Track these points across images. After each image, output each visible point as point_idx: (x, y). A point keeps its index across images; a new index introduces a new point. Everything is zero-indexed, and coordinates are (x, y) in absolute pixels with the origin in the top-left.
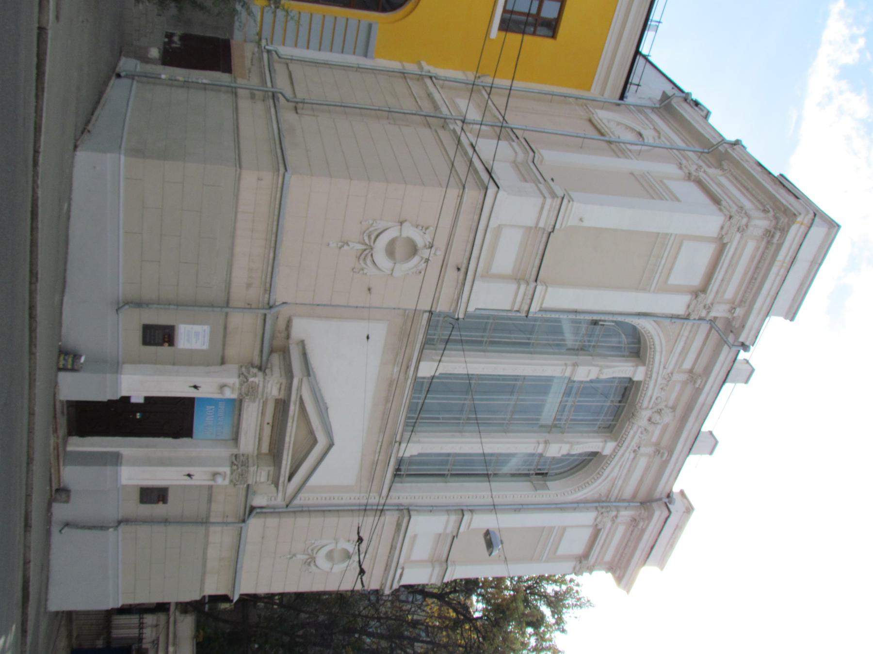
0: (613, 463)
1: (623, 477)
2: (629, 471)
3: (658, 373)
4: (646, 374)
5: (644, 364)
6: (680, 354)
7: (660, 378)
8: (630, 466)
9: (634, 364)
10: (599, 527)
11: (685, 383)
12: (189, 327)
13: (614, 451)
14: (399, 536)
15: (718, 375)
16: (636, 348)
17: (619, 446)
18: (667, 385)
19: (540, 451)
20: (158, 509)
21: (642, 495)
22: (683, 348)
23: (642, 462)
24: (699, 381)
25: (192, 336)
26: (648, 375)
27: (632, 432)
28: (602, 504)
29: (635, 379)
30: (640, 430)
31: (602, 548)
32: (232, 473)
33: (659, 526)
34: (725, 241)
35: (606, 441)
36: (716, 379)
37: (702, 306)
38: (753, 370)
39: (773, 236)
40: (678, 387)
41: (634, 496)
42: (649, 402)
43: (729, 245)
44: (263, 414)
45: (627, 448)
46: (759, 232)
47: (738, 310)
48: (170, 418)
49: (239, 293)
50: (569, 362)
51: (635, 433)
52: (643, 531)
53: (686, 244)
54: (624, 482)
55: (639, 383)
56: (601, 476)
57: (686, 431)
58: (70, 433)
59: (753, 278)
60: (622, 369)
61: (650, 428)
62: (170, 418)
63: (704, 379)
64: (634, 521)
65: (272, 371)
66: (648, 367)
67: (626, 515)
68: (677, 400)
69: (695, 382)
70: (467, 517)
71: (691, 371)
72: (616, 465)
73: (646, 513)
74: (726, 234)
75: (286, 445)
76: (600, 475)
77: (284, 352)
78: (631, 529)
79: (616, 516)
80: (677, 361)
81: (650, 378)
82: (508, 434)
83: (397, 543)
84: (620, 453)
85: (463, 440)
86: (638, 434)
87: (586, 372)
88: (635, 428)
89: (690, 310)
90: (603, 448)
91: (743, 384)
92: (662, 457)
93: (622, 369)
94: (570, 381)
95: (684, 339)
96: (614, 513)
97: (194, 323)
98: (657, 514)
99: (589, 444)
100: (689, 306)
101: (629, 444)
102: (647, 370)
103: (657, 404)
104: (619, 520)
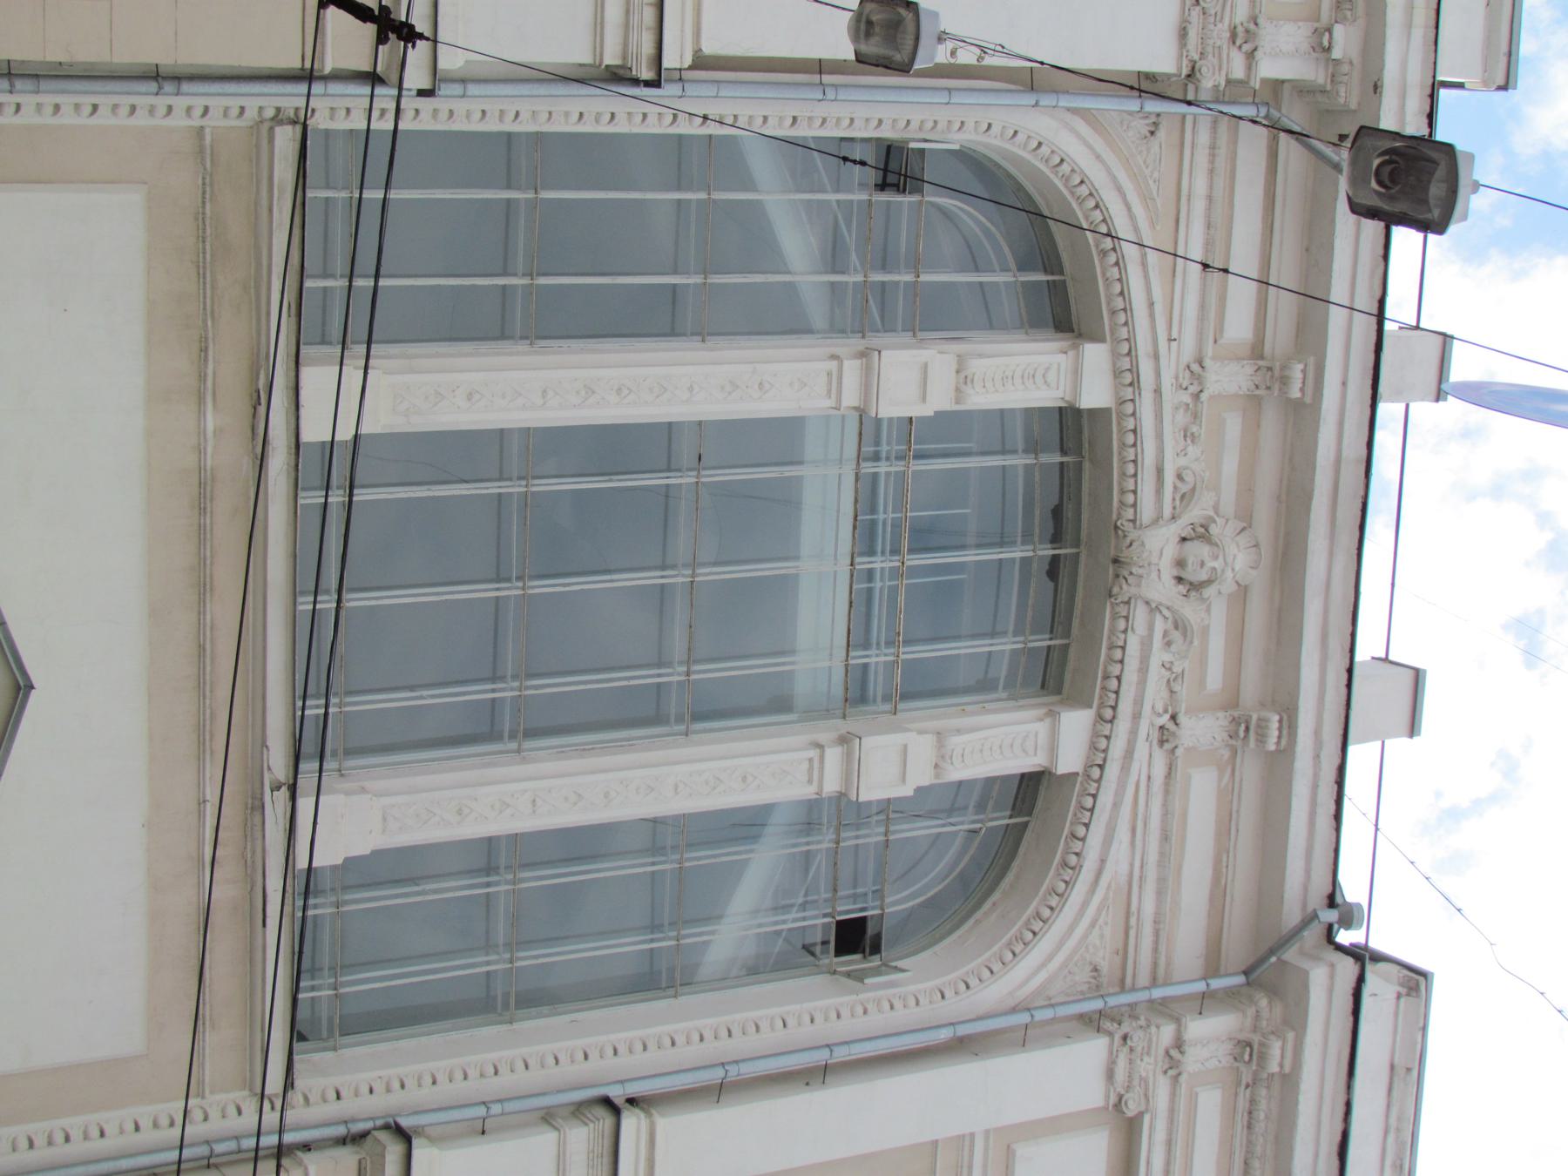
1: (1152, 874)
2: (1165, 838)
4: (1117, 373)
5: (1098, 338)
7: (1170, 360)
8: (1166, 813)
10: (1132, 1109)
11: (1253, 403)
13: (1093, 747)
15: (1317, 733)
16: (1052, 273)
17: (1105, 720)
18: (1196, 416)
19: (831, 785)
21: (1237, 949)
23: (1202, 788)
26: (1126, 375)
28: (1107, 1009)
29: (1086, 402)
34: (1130, 1114)
37: (1223, 30)
38: (1418, 676)
39: (1263, 1058)
40: (1234, 426)
41: (1212, 968)
43: (1147, 1118)
45: (1137, 716)
47: (1338, 30)
50: (823, 737)
51: (1146, 644)
52: (1289, 1082)
53: (1022, 1151)
54: (1160, 894)
56: (1076, 869)
57: (1301, 700)
60: (1023, 374)
64: (1247, 1050)
66: (1117, 341)
67: (1210, 1034)
68: (1247, 488)
69: (1284, 381)
70: (632, 1122)
71: (1257, 351)
72: (1116, 805)
73: (1278, 1010)
74: (1128, 1088)
78: (1242, 1104)
79: (1179, 1044)
80: (1203, 306)
81: (1135, 384)
82: (712, 342)
85: (530, 769)
86: (1158, 656)
87: (917, 378)
88: (1140, 615)
90: (1053, 749)
91: (1406, 740)
92: (1262, 738)
93: (1023, 374)
94: (869, 427)
95: (1199, 206)
96: (1167, 1033)
98: (1318, 976)
99: (1001, 740)
100: (1110, 1075)
101: (1139, 702)
102: (1115, 355)
103: (1186, 498)
104: (1193, 1060)
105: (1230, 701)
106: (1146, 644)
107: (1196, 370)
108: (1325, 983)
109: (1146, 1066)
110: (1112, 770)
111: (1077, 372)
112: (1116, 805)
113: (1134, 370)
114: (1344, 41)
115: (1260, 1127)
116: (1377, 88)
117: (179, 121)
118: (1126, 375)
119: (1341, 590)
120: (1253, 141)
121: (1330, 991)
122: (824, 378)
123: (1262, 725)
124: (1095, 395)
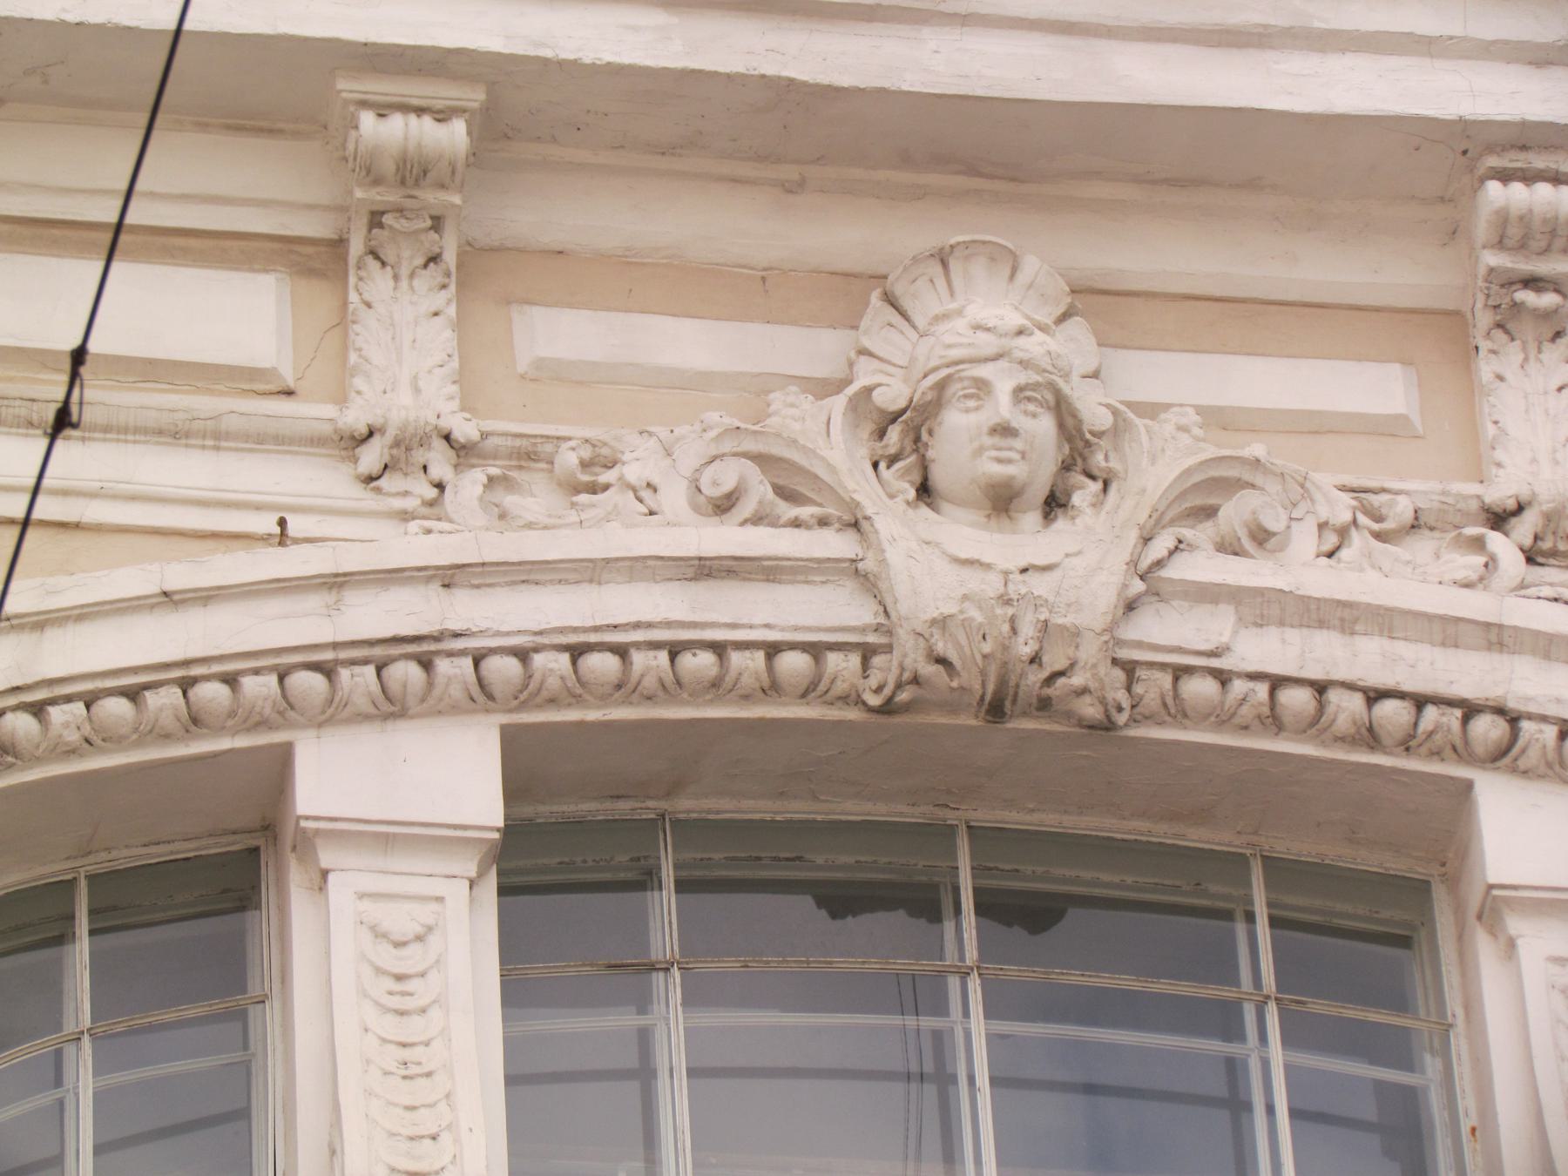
3: (337, 582)
4: (392, 708)
9: (297, 879)
11: (486, 274)
18: (529, 454)
24: (383, 133)
26: (398, 680)
29: (486, 807)
30: (1202, 566)
35: (1494, 908)
40: (558, 333)
42: (768, 571)
51: (1264, 608)
61: (1154, 468)
63: (349, 86)
66: (288, 708)
69: (414, 171)
71: (318, 261)
73: (332, 778)
77: (1413, 527)
80: (174, 434)
81: (424, 650)
86: (1298, 569)
88: (1168, 630)
101: (1449, 631)
102: (333, 714)
103: (792, 485)
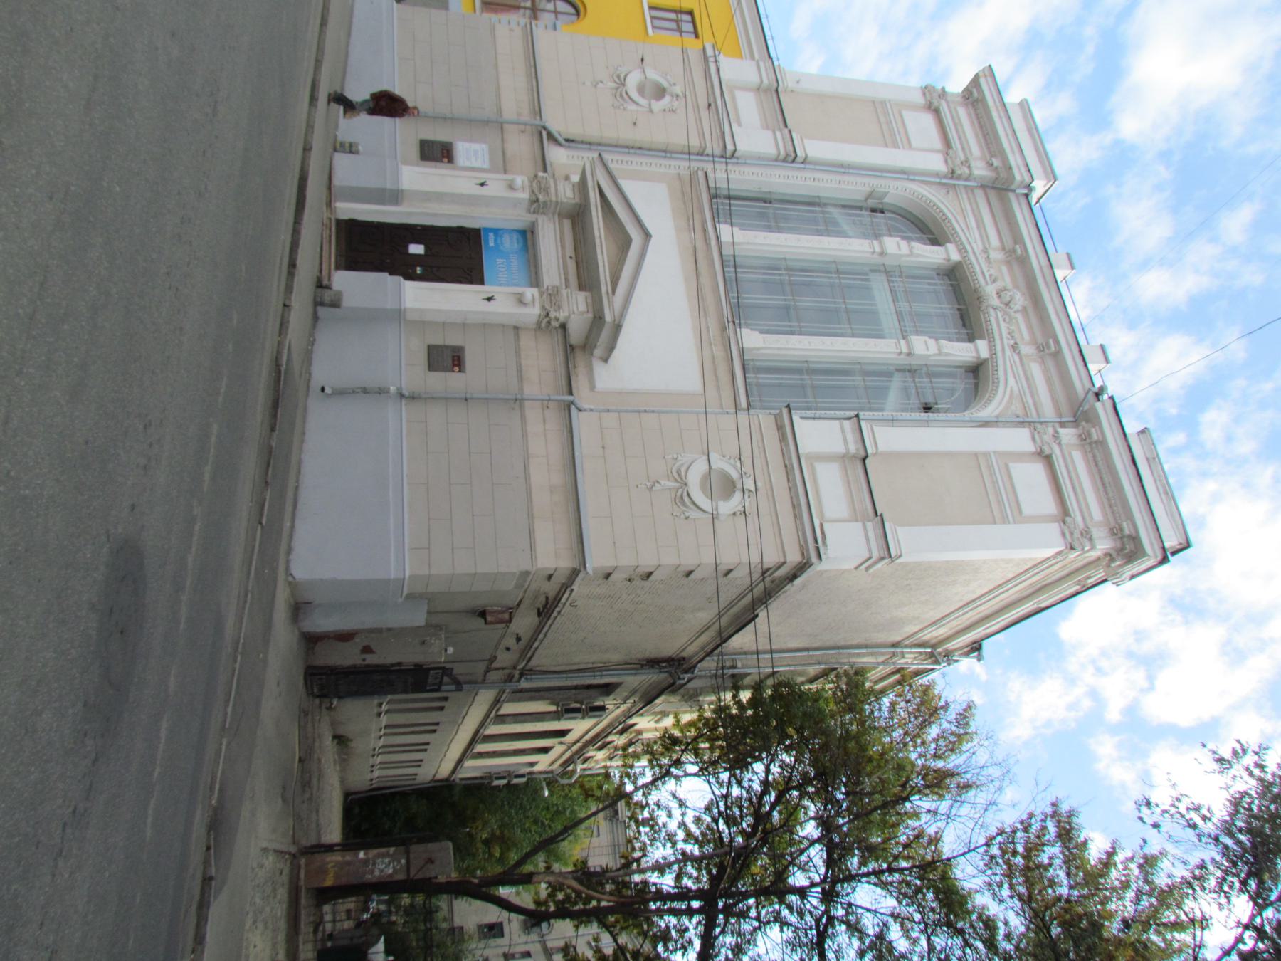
0: (1000, 362)
2: (1027, 379)
6: (978, 227)
12: (467, 145)
14: (787, 445)
17: (991, 341)
20: (452, 381)
22: (976, 221)
25: (470, 152)
26: (962, 249)
27: (993, 320)
31: (1075, 493)
32: (541, 296)
33: (1153, 534)
36: (1071, 350)
44: (563, 247)
46: (1075, 440)
48: (453, 253)
49: (509, 112)
51: (997, 319)
54: (1032, 396)
55: (986, 360)
58: (338, 268)
59: (985, 136)
62: (453, 253)
64: (1084, 438)
65: (536, 597)
72: (1006, 374)
75: (597, 241)
76: (996, 383)
78: (1091, 459)
81: (966, 251)
83: (790, 458)
84: (999, 348)
88: (992, 312)
89: (928, 97)
97: (471, 141)
102: (957, 246)
105: (1034, 341)
106: (997, 319)
107: (985, 251)
108: (1102, 409)
109: (1046, 437)
110: (999, 354)
111: (947, 252)
112: (1006, 374)
113: (964, 247)
114: (996, 162)
115: (1100, 463)
116: (1010, 168)
117: (672, 171)
118: (962, 249)
119: (1057, 300)
120: (979, 194)
121: (1105, 410)
122: (871, 571)
123: (1047, 344)
124: (955, 256)
